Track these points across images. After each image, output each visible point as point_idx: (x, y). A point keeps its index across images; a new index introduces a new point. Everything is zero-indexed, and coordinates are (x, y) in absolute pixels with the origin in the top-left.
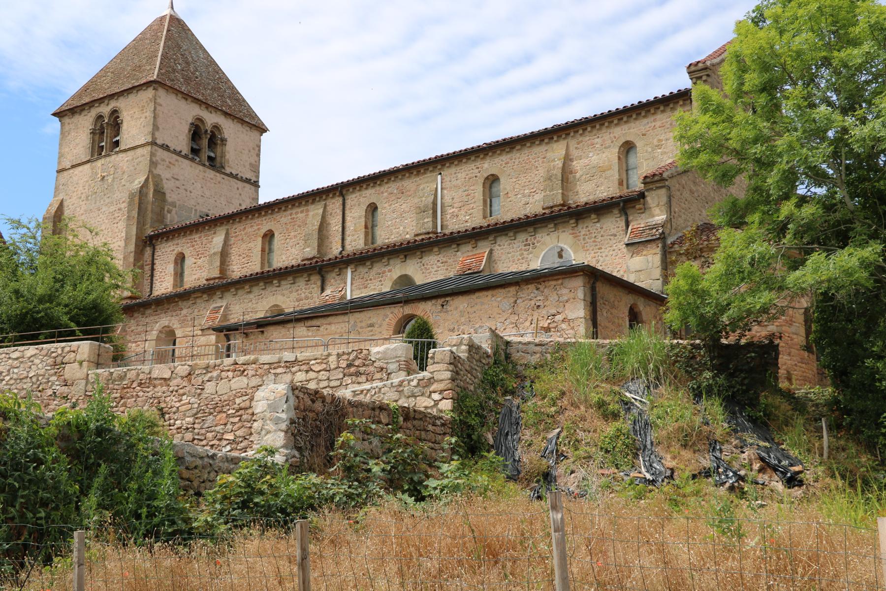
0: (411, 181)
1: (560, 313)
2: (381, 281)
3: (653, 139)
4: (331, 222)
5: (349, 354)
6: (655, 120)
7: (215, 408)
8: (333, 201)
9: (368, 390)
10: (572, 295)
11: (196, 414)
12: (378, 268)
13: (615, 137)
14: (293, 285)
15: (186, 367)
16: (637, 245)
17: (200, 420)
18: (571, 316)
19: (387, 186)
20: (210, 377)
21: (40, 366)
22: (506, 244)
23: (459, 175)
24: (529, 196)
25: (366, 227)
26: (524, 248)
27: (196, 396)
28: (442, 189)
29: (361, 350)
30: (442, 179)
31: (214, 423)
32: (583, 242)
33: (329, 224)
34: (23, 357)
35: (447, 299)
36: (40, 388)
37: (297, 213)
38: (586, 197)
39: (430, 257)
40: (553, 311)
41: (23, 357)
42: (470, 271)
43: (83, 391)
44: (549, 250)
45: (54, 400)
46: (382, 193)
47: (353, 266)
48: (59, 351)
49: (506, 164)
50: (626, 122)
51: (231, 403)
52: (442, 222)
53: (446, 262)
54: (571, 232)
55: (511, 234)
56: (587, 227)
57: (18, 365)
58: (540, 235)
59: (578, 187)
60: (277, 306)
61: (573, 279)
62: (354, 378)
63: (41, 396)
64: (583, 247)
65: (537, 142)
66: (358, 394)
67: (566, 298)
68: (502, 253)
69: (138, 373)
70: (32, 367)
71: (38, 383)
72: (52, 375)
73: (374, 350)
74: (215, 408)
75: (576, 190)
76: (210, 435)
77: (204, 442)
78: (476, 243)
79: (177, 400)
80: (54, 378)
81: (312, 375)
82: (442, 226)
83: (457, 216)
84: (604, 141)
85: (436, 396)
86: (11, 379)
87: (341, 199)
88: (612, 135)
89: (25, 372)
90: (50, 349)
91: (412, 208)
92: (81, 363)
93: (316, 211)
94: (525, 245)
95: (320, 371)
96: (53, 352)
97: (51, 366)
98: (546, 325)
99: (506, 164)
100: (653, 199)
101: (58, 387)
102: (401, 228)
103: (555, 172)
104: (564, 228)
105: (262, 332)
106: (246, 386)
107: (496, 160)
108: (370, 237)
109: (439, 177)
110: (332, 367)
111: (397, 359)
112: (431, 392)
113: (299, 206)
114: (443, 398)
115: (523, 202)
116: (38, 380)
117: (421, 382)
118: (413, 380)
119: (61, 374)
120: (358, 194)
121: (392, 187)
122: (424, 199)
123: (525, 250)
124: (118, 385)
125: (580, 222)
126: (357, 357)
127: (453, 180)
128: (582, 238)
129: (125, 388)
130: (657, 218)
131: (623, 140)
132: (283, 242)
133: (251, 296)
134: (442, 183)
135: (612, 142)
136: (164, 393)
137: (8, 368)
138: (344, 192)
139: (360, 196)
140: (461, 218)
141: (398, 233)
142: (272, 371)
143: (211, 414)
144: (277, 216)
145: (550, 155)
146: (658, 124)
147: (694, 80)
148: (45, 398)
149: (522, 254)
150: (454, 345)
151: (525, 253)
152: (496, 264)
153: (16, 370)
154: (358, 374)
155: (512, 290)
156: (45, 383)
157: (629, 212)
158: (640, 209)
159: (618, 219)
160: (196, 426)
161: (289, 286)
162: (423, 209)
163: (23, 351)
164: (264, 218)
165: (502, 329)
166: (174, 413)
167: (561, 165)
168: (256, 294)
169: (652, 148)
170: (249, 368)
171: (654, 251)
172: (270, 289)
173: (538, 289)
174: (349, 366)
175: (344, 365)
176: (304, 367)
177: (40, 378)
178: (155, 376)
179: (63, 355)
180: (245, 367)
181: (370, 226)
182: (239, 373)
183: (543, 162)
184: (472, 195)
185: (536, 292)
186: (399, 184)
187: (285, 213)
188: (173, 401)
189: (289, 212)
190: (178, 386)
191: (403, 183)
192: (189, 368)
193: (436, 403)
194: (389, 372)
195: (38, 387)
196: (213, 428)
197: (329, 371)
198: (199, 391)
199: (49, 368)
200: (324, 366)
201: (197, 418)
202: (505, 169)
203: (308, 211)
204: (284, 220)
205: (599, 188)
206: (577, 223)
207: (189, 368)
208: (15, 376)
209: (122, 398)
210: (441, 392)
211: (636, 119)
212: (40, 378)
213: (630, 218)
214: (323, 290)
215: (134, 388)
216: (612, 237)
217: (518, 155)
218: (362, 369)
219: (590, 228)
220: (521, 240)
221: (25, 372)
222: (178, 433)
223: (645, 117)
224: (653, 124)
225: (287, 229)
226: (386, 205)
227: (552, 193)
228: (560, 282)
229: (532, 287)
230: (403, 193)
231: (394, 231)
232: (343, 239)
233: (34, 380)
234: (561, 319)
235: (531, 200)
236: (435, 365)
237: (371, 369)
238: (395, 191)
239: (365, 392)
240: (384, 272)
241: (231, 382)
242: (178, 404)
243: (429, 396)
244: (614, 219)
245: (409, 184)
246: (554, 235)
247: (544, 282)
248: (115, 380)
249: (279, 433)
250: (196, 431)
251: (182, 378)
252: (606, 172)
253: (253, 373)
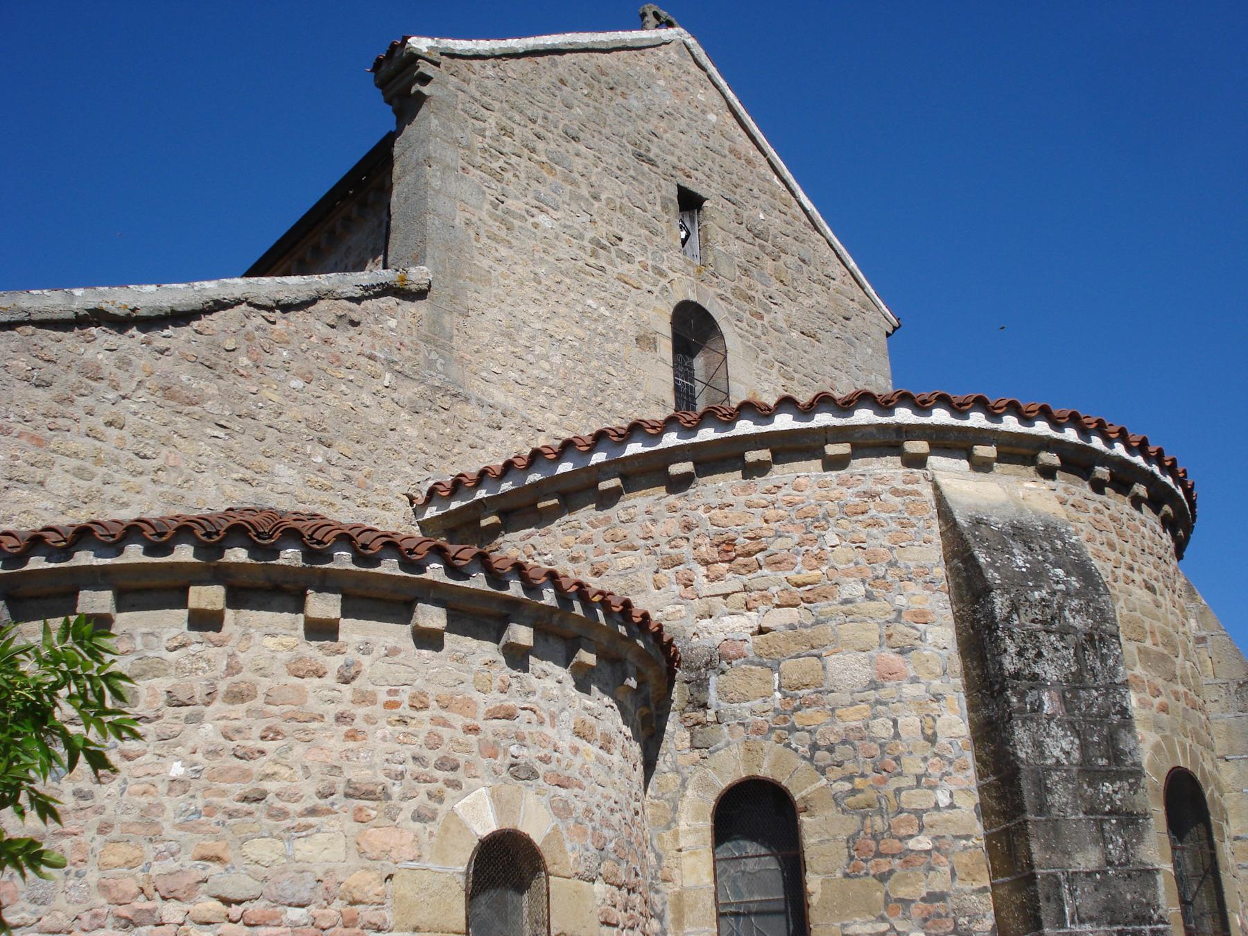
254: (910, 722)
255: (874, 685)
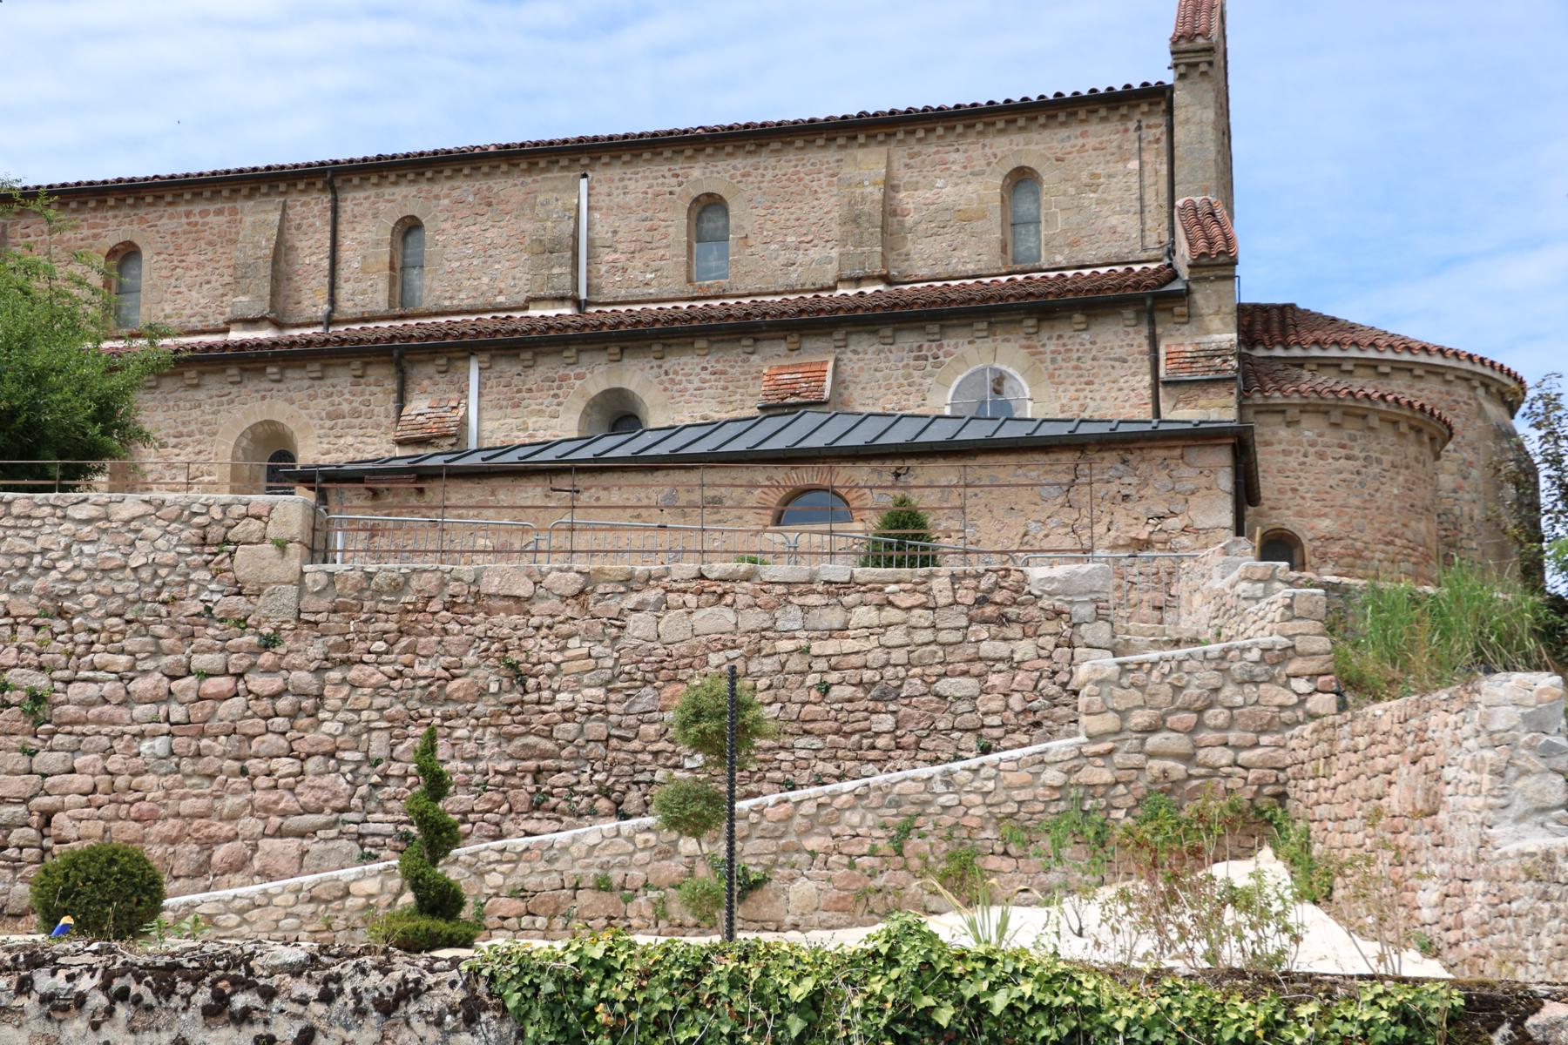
0: (510, 182)
1: (1176, 515)
2: (556, 396)
3: (1080, 170)
4: (298, 244)
5: (978, 576)
6: (1084, 134)
7: (656, 671)
8: (304, 198)
9: (1154, 664)
10: (1203, 481)
11: (609, 682)
12: (547, 368)
13: (995, 156)
14: (316, 383)
15: (572, 575)
16: (1186, 387)
17: (620, 696)
18: (1202, 521)
19: (449, 184)
20: (639, 603)
21: (161, 543)
22: (871, 350)
23: (632, 185)
24: (797, 249)
25: (392, 268)
26: (912, 363)
27: (607, 642)
28: (589, 208)
29: (1007, 570)
30: (590, 188)
31: (659, 705)
32: (1051, 367)
33: (293, 248)
34: (107, 518)
35: (909, 463)
36: (164, 595)
37: (204, 213)
38: (926, 266)
39: (683, 359)
40: (1161, 509)
41: (107, 518)
42: (797, 399)
43: (295, 613)
44: (973, 374)
45: (206, 626)
46: (437, 197)
47: (485, 357)
48: (216, 513)
49: (743, 175)
50: (1022, 129)
51: (696, 662)
52: (588, 278)
53: (723, 373)
54: (1024, 342)
55: (888, 332)
56: (1060, 337)
57: (95, 536)
58: (952, 342)
59: (910, 245)
60: (270, 423)
61: (1209, 450)
62: (994, 628)
63: (169, 614)
64: (1051, 376)
65: (820, 142)
66: (1131, 671)
67: (1190, 486)
68: (861, 369)
69: (442, 578)
70: (138, 543)
71: (158, 582)
72: (196, 568)
73: (1038, 573)
74: (656, 671)
75: (904, 251)
76: (650, 730)
77: (636, 745)
78: (799, 342)
79: (552, 647)
80: (203, 575)
81: (891, 614)
82: (588, 286)
83: (624, 270)
84: (970, 159)
85: (1302, 686)
86: (75, 567)
87: (326, 199)
88: (988, 151)
89: (117, 555)
90: (189, 506)
91: (513, 241)
92: (282, 546)
93: (263, 216)
94: (917, 358)
95: (909, 609)
96: (195, 514)
97: (192, 545)
98: (1144, 536)
99: (743, 175)
100: (1207, 298)
101: (216, 597)
102: (485, 280)
103: (866, 208)
104: (1008, 332)
105: (421, 491)
106: (732, 628)
107: (721, 165)
108: (398, 289)
109: (584, 182)
110: (942, 601)
111: (1094, 596)
112: (1288, 676)
113: (211, 200)
114: (1317, 690)
115: (782, 260)
116: (155, 575)
117: (1267, 655)
118: (1249, 650)
119: (225, 566)
120: (372, 192)
121: (465, 188)
122: (549, 224)
123: (916, 368)
124: (391, 602)
125: (1044, 324)
126: (997, 586)
127: (616, 193)
128: (1048, 357)
129: (409, 611)
130: (1216, 337)
131: (1013, 164)
132: (165, 273)
133: (201, 395)
134: (589, 195)
135: (989, 164)
136: (515, 628)
137: (63, 541)
138: (338, 183)
139: (377, 196)
140: (631, 274)
141: (476, 289)
142: (796, 600)
143: (646, 682)
144: (152, 214)
145: (847, 171)
146: (1091, 142)
147: (1182, 69)
148: (182, 619)
149: (910, 375)
150: (1259, 580)
151: (916, 373)
152: (846, 388)
153: (87, 549)
154: (1003, 620)
155: (1067, 458)
156: (178, 584)
157: (1159, 317)
158: (1182, 316)
159: (1131, 330)
160: (611, 707)
161: (307, 383)
162: (549, 246)
163: (106, 505)
164: (110, 214)
165: (1040, 535)
166: (550, 676)
167: (878, 196)
168: (214, 392)
169: (1077, 188)
170: (737, 590)
171: (1223, 402)
172: (253, 385)
173: (1124, 462)
174: (982, 601)
175: (970, 600)
176: (874, 598)
177: (163, 572)
178: (492, 590)
179: (229, 522)
180: (728, 585)
181: (398, 266)
182: (712, 599)
183: (830, 184)
184: (662, 230)
185: (1121, 467)
186: (481, 184)
187: (170, 210)
188: (540, 647)
189: (182, 209)
190: (552, 616)
191: (491, 183)
192: (581, 579)
193: (1303, 698)
194: (1075, 620)
195: (158, 594)
196: (656, 715)
197: (933, 609)
198: (614, 631)
199: (188, 550)
200: (923, 598)
201: (609, 691)
202: (741, 186)
203: (234, 212)
204: (167, 224)
205: (957, 253)
206: (1038, 327)
207: (581, 579)
208: (87, 562)
209: (401, 632)
210: (1312, 677)
211: (1044, 126)
212: (163, 572)
213: (1159, 330)
214: (401, 402)
215: (434, 613)
216: (1117, 364)
217: (772, 161)
218: (1012, 611)
219: (1065, 340)
220: (907, 346)
221: (117, 555)
222: (566, 721)
223: (1063, 124)
224: (1080, 141)
225: (178, 247)
226: (447, 225)
227: (859, 250)
228: (1177, 452)
229: (1111, 458)
230: (490, 205)
231: (466, 283)
232: (333, 286)
233: (145, 574)
234: (1180, 526)
235: (800, 257)
236: (1295, 622)
237: (1033, 611)
238: (470, 199)
239: (1147, 666)
240: (564, 379)
241: (694, 617)
242: (557, 658)
243: (1286, 685)
244: (1120, 328)
245: (508, 187)
246: (986, 345)
247: (1141, 449)
248: (379, 592)
249: (1551, 776)
250: (613, 718)
251: (563, 598)
252: (974, 224)
253: (749, 600)
254: (1466, 509)
255: (1455, 491)
